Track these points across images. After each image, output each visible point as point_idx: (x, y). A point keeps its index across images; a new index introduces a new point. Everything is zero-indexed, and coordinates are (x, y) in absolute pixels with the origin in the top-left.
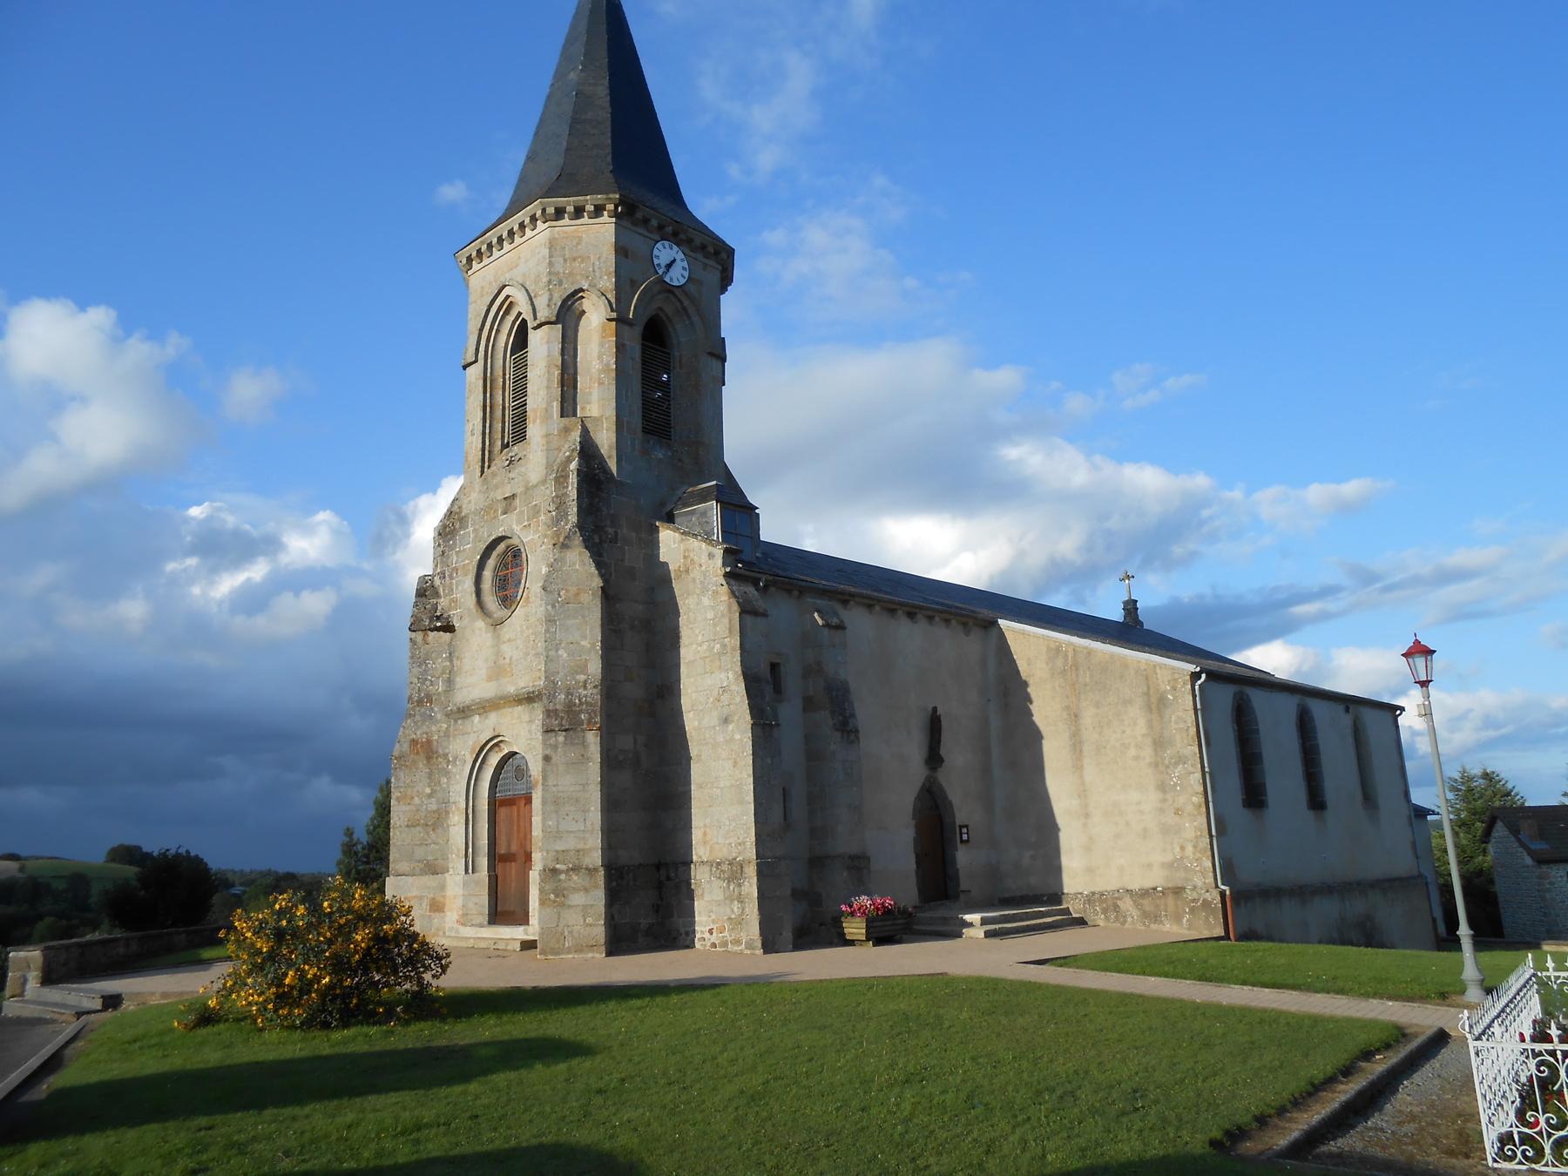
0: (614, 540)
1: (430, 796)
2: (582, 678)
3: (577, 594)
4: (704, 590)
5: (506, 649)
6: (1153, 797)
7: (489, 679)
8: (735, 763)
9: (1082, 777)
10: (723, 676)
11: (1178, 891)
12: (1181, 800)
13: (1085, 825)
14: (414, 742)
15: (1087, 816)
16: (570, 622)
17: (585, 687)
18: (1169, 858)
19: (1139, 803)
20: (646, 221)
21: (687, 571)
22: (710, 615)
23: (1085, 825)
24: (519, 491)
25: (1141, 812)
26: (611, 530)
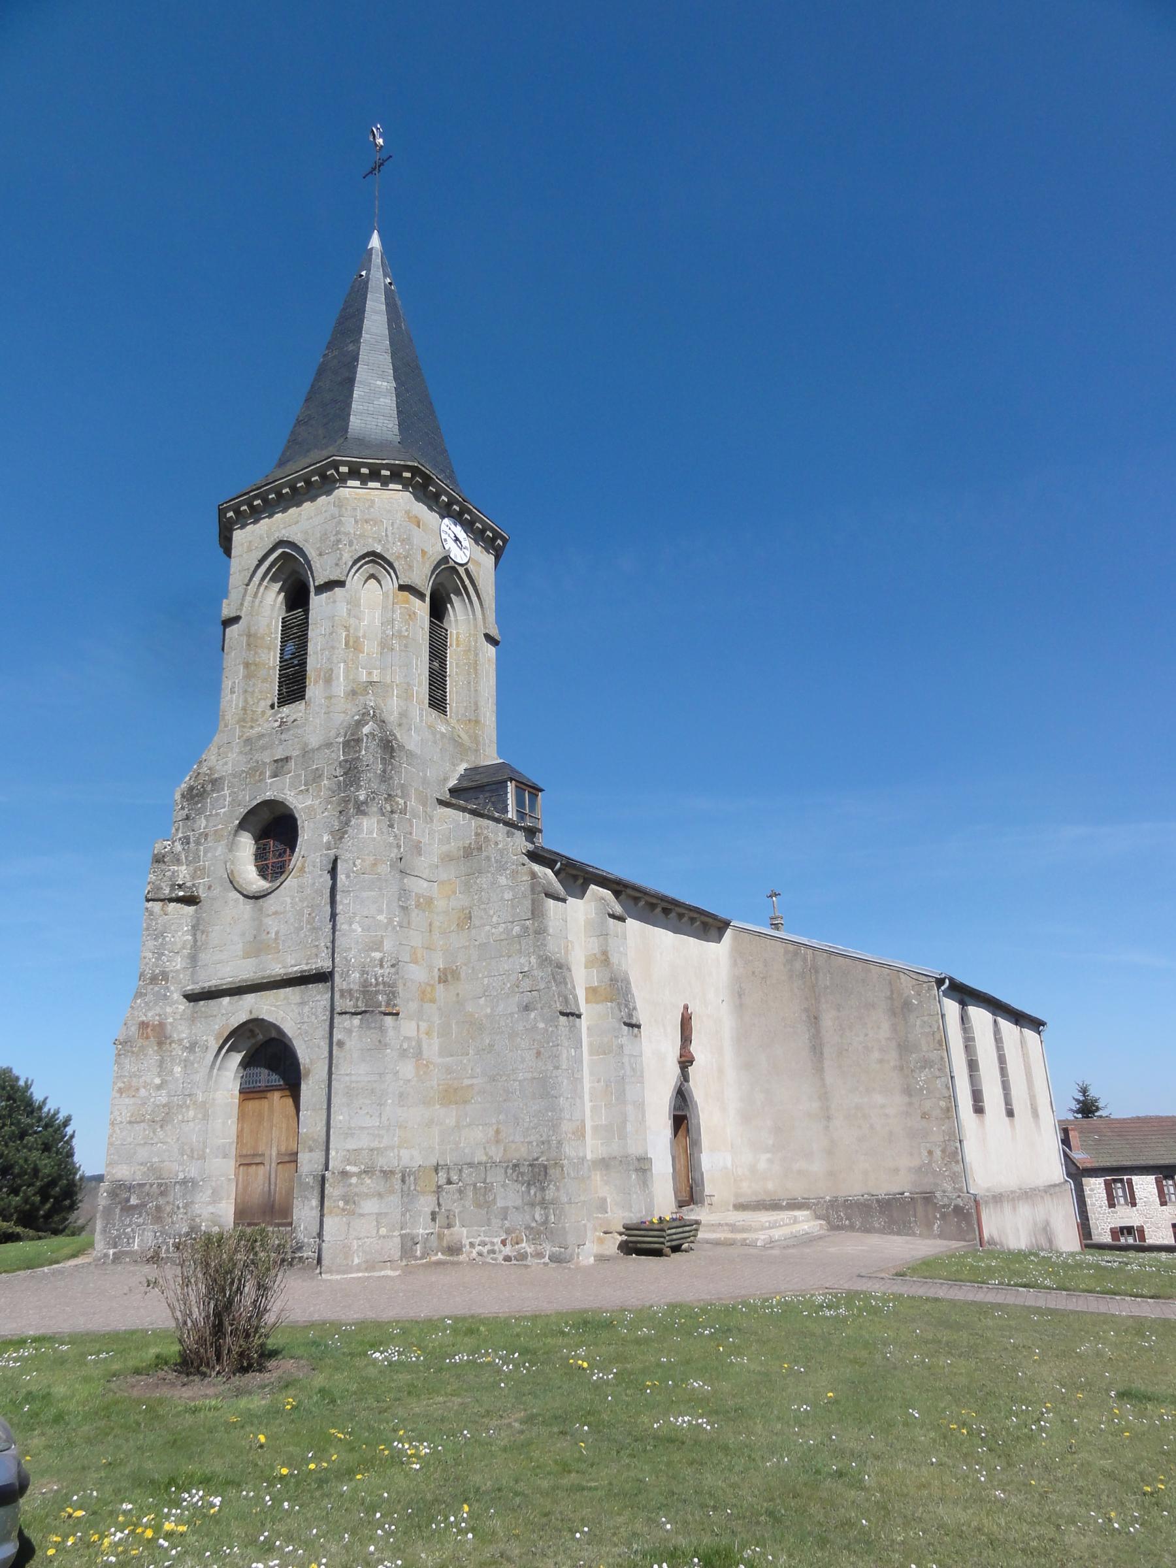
0: (404, 812)
1: (159, 1087)
2: (377, 955)
3: (375, 865)
4: (502, 868)
5: (273, 925)
6: (900, 1100)
7: (247, 955)
8: (538, 1054)
9: (823, 1079)
10: (523, 960)
11: (928, 1198)
12: (928, 1104)
13: (827, 1128)
14: (143, 1025)
15: (829, 1118)
16: (365, 894)
17: (381, 966)
18: (916, 1162)
19: (883, 1106)
20: (437, 496)
21: (480, 849)
22: (508, 895)
23: (827, 1128)
24: (295, 753)
25: (887, 1115)
26: (401, 801)
